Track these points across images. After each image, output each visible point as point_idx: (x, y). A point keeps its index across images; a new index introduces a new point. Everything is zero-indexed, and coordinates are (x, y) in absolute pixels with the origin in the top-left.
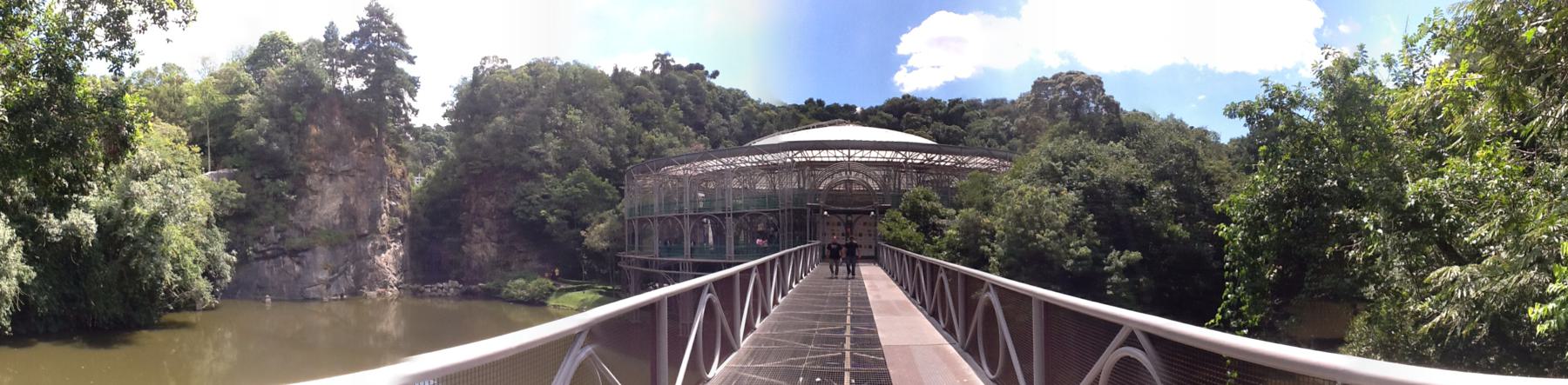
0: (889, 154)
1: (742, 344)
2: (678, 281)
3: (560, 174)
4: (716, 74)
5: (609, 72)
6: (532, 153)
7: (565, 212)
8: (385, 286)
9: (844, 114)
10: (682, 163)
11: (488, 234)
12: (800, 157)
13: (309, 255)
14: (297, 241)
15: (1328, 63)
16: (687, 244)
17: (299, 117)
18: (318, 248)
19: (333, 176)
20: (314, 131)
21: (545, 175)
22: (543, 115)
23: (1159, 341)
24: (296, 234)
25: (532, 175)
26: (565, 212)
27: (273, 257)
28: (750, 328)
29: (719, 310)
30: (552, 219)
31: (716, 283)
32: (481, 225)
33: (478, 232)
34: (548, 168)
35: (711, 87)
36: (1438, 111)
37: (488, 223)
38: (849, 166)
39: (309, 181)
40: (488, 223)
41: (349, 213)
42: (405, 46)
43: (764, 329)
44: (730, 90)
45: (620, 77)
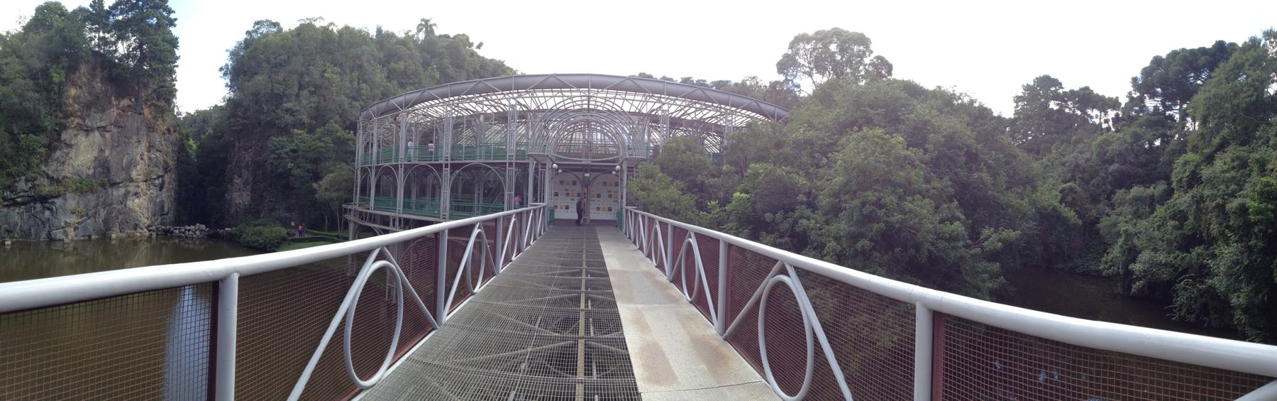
1: (446, 317)
3: (311, 130)
4: (479, 46)
6: (287, 110)
7: (309, 166)
8: (136, 227)
11: (246, 183)
13: (58, 201)
14: (46, 188)
17: (56, 78)
18: (68, 195)
19: (88, 131)
20: (73, 91)
21: (296, 131)
22: (302, 75)
24: (45, 182)
25: (285, 130)
26: (309, 166)
27: (23, 204)
28: (507, 260)
29: (485, 240)
30: (296, 172)
32: (240, 176)
33: (237, 181)
34: (301, 125)
35: (473, 54)
37: (245, 174)
38: (588, 118)
39: (64, 136)
40: (245, 174)
41: (103, 166)
42: (170, 11)
43: (486, 295)
44: (492, 60)
45: (384, 38)
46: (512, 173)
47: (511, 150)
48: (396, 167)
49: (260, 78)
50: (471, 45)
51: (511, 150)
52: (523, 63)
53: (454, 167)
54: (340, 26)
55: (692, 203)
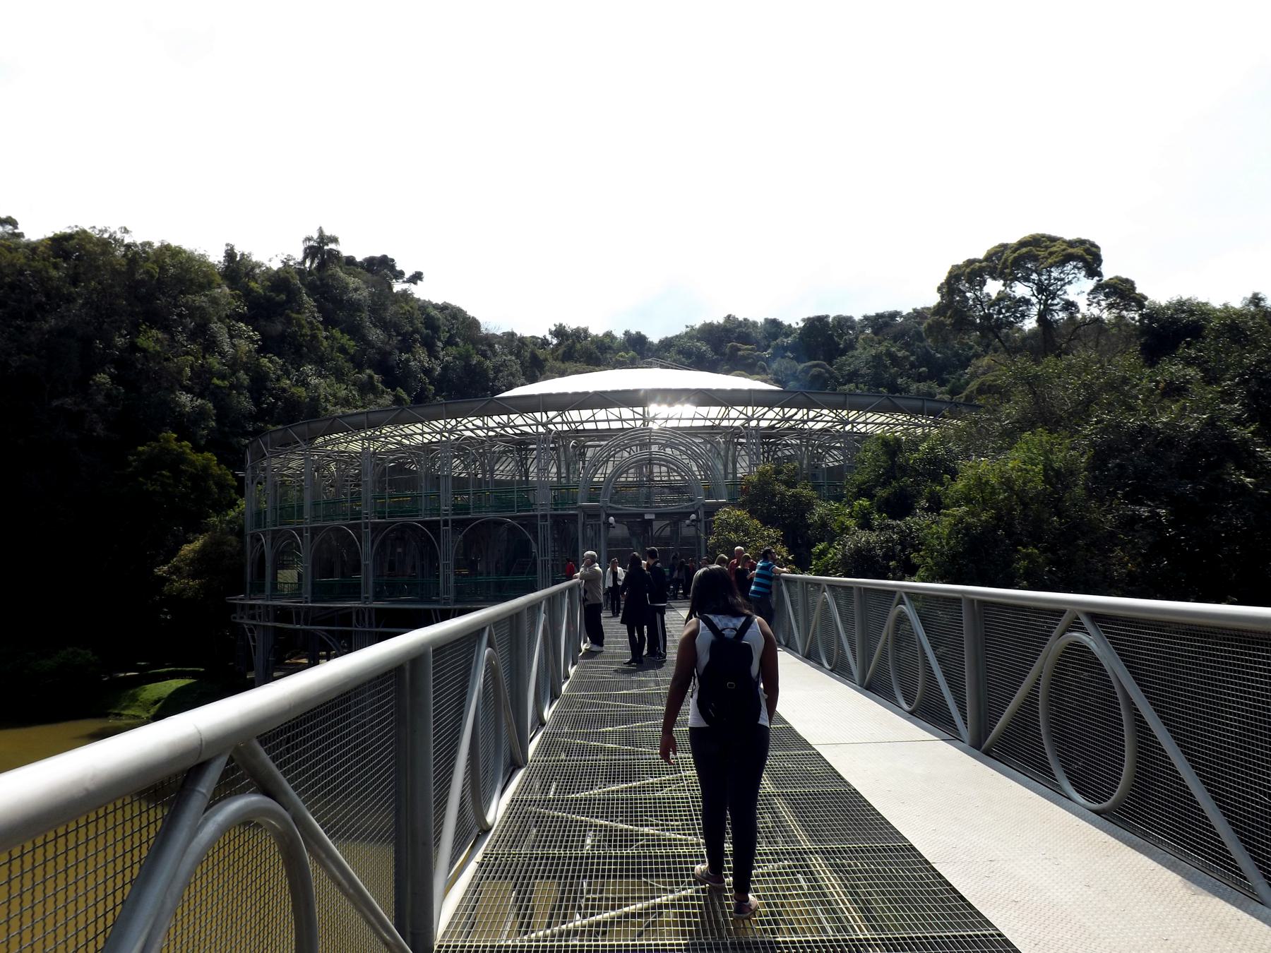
0: (714, 411)
2: (350, 650)
4: (417, 277)
5: (216, 257)
9: (637, 350)
10: (359, 427)
12: (558, 422)
15: (119, 236)
16: (367, 577)
23: (1099, 618)
31: (497, 622)
36: (922, 544)
45: (237, 268)
46: (545, 528)
47: (543, 503)
48: (433, 526)
50: (400, 275)
51: (543, 503)
52: (508, 305)
54: (157, 245)
55: (352, 351)
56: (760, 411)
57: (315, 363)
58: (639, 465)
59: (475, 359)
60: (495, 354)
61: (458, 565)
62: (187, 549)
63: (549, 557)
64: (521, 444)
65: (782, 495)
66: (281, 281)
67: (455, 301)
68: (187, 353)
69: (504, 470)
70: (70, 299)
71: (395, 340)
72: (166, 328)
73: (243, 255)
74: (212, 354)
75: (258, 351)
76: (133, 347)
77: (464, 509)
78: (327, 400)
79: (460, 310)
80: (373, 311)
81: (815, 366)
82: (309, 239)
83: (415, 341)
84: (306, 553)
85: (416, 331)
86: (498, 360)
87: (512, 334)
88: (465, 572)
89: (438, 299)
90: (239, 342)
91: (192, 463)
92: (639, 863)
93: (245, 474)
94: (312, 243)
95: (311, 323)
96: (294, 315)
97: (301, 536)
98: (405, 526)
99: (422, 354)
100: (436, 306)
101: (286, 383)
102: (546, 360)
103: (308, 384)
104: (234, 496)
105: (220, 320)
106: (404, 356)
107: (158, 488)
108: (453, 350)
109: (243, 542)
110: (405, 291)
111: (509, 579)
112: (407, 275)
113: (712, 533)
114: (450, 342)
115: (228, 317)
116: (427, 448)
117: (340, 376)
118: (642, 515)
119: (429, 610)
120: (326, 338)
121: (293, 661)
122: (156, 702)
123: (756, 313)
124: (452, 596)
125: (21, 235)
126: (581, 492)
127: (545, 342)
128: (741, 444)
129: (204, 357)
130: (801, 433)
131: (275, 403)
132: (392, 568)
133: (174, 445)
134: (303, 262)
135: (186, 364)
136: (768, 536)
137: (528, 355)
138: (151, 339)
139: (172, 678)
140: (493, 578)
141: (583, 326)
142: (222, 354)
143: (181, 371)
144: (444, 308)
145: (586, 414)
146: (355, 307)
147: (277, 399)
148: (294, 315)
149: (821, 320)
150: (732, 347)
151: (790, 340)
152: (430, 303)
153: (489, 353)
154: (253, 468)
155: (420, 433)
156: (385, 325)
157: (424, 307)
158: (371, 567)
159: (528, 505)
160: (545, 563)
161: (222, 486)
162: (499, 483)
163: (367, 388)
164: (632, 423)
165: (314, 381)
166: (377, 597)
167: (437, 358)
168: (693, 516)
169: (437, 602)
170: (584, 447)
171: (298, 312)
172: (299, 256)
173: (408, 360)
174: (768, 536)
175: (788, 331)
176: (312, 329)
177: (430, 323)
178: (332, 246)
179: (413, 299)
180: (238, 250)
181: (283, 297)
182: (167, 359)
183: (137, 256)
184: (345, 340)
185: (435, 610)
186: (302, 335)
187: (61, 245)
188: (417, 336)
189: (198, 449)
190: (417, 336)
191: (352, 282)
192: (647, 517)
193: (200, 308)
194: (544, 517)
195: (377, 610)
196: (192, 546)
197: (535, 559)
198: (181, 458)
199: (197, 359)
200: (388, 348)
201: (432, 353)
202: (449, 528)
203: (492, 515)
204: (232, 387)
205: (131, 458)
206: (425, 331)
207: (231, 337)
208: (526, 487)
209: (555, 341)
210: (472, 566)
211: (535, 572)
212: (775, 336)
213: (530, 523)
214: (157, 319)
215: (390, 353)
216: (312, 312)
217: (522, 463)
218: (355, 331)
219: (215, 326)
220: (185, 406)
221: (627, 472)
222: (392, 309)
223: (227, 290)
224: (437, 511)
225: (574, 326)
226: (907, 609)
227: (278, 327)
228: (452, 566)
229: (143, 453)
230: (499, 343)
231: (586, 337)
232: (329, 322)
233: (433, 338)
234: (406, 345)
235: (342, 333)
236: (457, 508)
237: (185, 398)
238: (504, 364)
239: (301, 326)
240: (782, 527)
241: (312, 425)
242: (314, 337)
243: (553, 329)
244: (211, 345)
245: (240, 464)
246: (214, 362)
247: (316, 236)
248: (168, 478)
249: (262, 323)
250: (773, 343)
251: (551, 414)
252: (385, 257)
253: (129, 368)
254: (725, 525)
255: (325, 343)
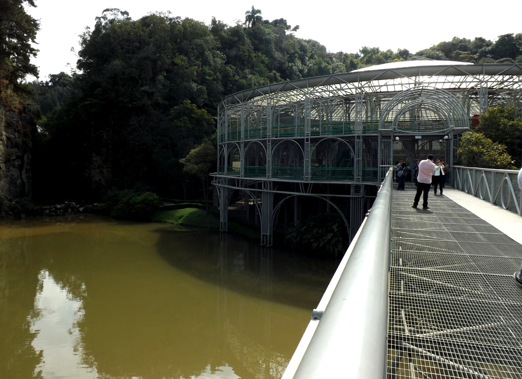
4: (296, 28)
5: (208, 23)
16: (269, 167)
45: (217, 27)
46: (359, 145)
47: (358, 131)
48: (301, 141)
49: (117, 63)
50: (288, 27)
51: (358, 131)
52: (340, 41)
53: (313, 141)
54: (183, 18)
55: (266, 62)
56: (487, 78)
57: (250, 68)
58: (412, 110)
59: (324, 65)
60: (333, 62)
61: (313, 161)
62: (193, 151)
63: (361, 158)
64: (347, 100)
65: (505, 125)
66: (236, 31)
67: (314, 38)
68: (195, 65)
69: (337, 116)
70: (148, 44)
71: (287, 57)
72: (186, 55)
73: (219, 21)
74: (206, 65)
75: (226, 64)
76: (174, 64)
77: (318, 133)
78: (255, 85)
79: (317, 42)
80: (276, 44)
81: (507, 60)
82: (248, 12)
83: (295, 57)
84: (242, 153)
85: (296, 52)
86: (335, 64)
87: (341, 53)
88: (317, 165)
89: (306, 38)
90: (218, 60)
91: (196, 113)
92: (393, 282)
93: (218, 118)
94: (249, 14)
95: (249, 50)
96: (241, 47)
97: (240, 146)
98: (287, 142)
99: (299, 63)
100: (305, 41)
101: (237, 77)
102: (358, 64)
103: (247, 78)
104: (214, 128)
105: (209, 50)
106: (290, 64)
107: (182, 124)
108: (313, 61)
109: (216, 148)
110: (291, 34)
111: (340, 169)
112: (292, 28)
113: (460, 146)
114: (311, 57)
115: (213, 49)
116: (300, 104)
117: (261, 74)
118: (414, 136)
119: (298, 184)
120: (255, 57)
121: (239, 202)
122: (181, 217)
123: (470, 36)
124: (310, 177)
125: (130, 18)
126: (380, 124)
127: (357, 56)
128: (472, 98)
129: (202, 67)
130: (511, 92)
131: (232, 87)
132: (282, 162)
133: (189, 106)
134: (245, 23)
135: (194, 70)
136: (497, 149)
137: (349, 62)
138: (180, 60)
139: (188, 207)
140: (330, 168)
141: (376, 47)
142: (210, 65)
143: (192, 74)
144: (309, 41)
145: (382, 82)
146: (268, 42)
147: (233, 85)
148: (241, 47)
149: (509, 36)
150: (456, 53)
151: (490, 48)
152: (302, 39)
153: (330, 62)
154: (220, 115)
155: (296, 96)
156: (281, 50)
157: (299, 41)
158: (271, 161)
159: (350, 131)
160: (358, 161)
161: (209, 124)
162: (335, 123)
163: (273, 79)
164: (407, 86)
165: (250, 76)
166: (275, 175)
167: (305, 65)
168: (446, 137)
169: (302, 179)
170: (380, 101)
171: (243, 45)
172: (244, 20)
173: (292, 66)
174: (497, 149)
175: (489, 44)
176: (249, 53)
177: (303, 49)
178: (258, 15)
179: (294, 38)
180: (217, 19)
181: (236, 38)
182: (187, 68)
183: (173, 24)
184: (264, 57)
185: (301, 183)
186: (245, 56)
187: (146, 21)
188: (297, 55)
189: (199, 107)
190: (297, 55)
191: (267, 30)
192: (416, 137)
193: (201, 45)
194: (358, 137)
195: (274, 182)
196: (195, 150)
197: (353, 159)
198: (192, 111)
199: (199, 67)
200: (283, 61)
201: (303, 62)
202: (309, 142)
203: (331, 136)
204: (214, 80)
205: (172, 111)
206: (300, 52)
207: (214, 57)
208: (349, 123)
209: (362, 55)
210: (320, 162)
211: (353, 166)
212: (481, 47)
213: (351, 140)
214: (182, 51)
215: (284, 63)
216: (249, 45)
217: (347, 112)
218: (268, 53)
219: (207, 53)
220: (194, 88)
221: (404, 113)
222: (285, 42)
223: (212, 37)
224: (302, 134)
225: (372, 48)
226: (507, 178)
227: (233, 52)
228: (310, 162)
229: (176, 109)
230: (335, 57)
231: (378, 53)
232: (257, 49)
233: (304, 55)
234: (291, 59)
235: (262, 54)
236: (313, 133)
237: (194, 85)
238: (337, 67)
239: (244, 52)
240: (507, 144)
241: (245, 93)
242: (250, 56)
243: (361, 49)
244: (206, 62)
245: (215, 114)
246: (207, 69)
247: (251, 10)
248: (187, 120)
249: (227, 50)
250: (480, 50)
251: (363, 83)
252: (282, 19)
253: (172, 72)
254: (469, 141)
255: (255, 59)
